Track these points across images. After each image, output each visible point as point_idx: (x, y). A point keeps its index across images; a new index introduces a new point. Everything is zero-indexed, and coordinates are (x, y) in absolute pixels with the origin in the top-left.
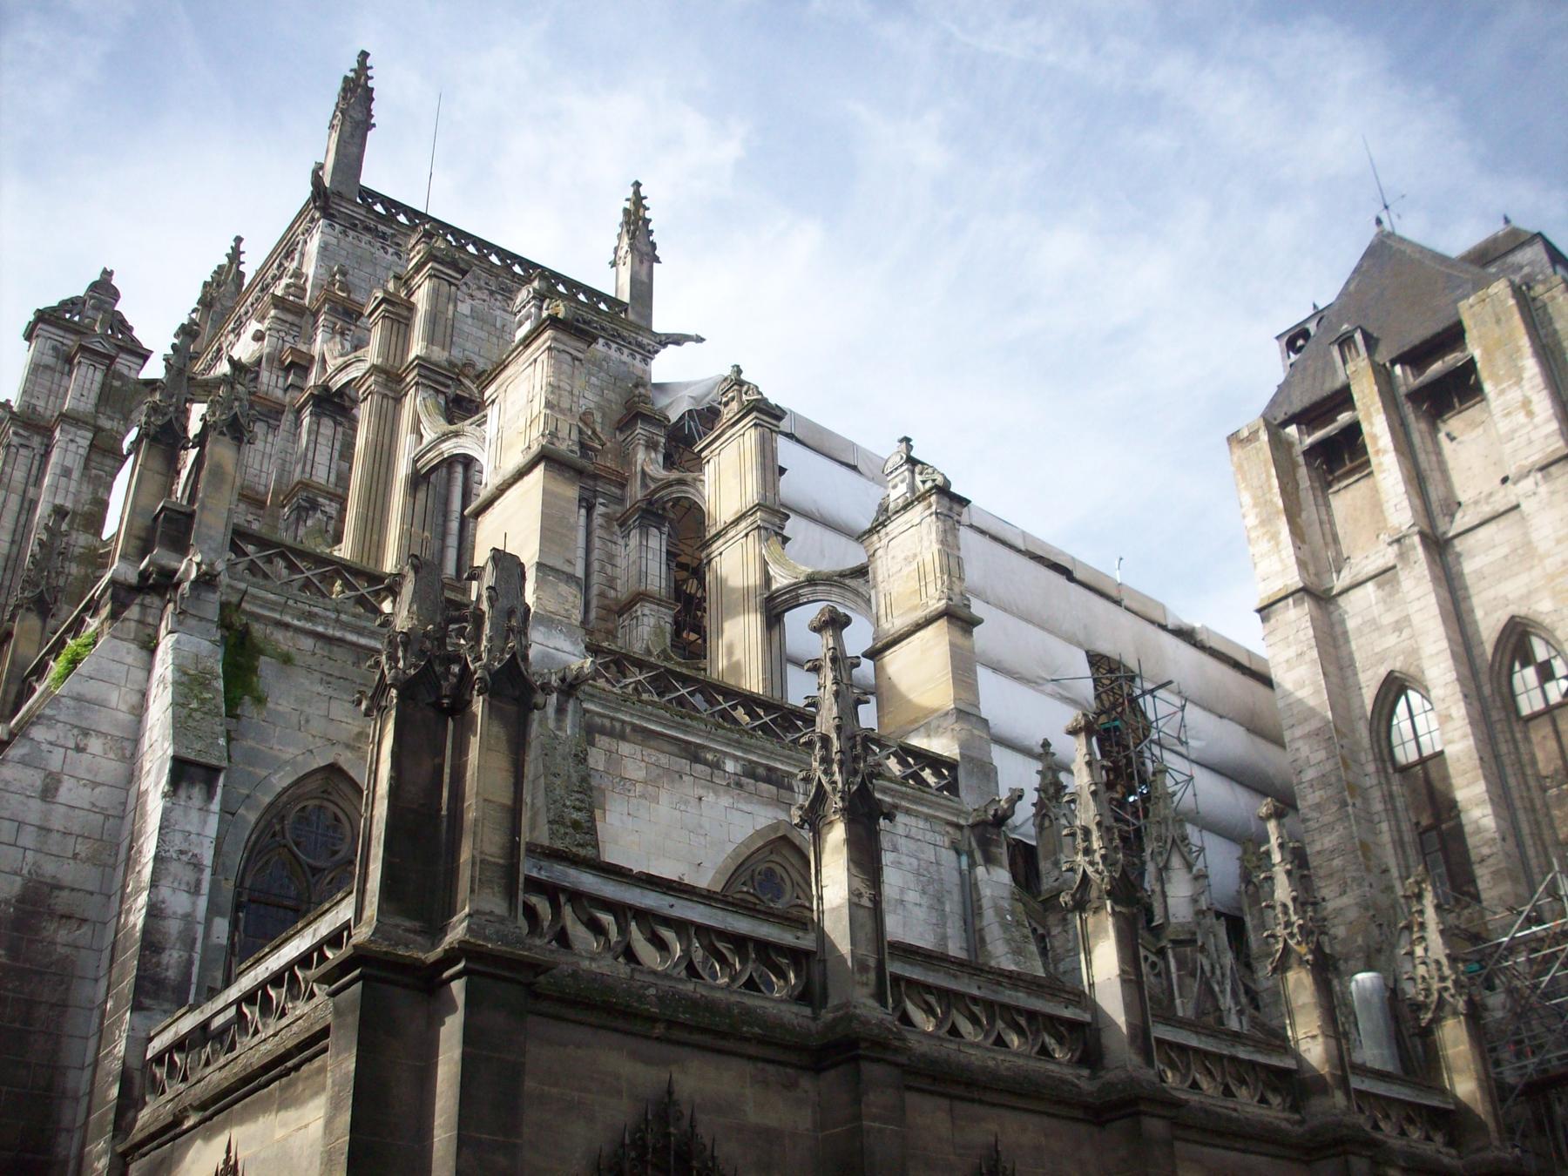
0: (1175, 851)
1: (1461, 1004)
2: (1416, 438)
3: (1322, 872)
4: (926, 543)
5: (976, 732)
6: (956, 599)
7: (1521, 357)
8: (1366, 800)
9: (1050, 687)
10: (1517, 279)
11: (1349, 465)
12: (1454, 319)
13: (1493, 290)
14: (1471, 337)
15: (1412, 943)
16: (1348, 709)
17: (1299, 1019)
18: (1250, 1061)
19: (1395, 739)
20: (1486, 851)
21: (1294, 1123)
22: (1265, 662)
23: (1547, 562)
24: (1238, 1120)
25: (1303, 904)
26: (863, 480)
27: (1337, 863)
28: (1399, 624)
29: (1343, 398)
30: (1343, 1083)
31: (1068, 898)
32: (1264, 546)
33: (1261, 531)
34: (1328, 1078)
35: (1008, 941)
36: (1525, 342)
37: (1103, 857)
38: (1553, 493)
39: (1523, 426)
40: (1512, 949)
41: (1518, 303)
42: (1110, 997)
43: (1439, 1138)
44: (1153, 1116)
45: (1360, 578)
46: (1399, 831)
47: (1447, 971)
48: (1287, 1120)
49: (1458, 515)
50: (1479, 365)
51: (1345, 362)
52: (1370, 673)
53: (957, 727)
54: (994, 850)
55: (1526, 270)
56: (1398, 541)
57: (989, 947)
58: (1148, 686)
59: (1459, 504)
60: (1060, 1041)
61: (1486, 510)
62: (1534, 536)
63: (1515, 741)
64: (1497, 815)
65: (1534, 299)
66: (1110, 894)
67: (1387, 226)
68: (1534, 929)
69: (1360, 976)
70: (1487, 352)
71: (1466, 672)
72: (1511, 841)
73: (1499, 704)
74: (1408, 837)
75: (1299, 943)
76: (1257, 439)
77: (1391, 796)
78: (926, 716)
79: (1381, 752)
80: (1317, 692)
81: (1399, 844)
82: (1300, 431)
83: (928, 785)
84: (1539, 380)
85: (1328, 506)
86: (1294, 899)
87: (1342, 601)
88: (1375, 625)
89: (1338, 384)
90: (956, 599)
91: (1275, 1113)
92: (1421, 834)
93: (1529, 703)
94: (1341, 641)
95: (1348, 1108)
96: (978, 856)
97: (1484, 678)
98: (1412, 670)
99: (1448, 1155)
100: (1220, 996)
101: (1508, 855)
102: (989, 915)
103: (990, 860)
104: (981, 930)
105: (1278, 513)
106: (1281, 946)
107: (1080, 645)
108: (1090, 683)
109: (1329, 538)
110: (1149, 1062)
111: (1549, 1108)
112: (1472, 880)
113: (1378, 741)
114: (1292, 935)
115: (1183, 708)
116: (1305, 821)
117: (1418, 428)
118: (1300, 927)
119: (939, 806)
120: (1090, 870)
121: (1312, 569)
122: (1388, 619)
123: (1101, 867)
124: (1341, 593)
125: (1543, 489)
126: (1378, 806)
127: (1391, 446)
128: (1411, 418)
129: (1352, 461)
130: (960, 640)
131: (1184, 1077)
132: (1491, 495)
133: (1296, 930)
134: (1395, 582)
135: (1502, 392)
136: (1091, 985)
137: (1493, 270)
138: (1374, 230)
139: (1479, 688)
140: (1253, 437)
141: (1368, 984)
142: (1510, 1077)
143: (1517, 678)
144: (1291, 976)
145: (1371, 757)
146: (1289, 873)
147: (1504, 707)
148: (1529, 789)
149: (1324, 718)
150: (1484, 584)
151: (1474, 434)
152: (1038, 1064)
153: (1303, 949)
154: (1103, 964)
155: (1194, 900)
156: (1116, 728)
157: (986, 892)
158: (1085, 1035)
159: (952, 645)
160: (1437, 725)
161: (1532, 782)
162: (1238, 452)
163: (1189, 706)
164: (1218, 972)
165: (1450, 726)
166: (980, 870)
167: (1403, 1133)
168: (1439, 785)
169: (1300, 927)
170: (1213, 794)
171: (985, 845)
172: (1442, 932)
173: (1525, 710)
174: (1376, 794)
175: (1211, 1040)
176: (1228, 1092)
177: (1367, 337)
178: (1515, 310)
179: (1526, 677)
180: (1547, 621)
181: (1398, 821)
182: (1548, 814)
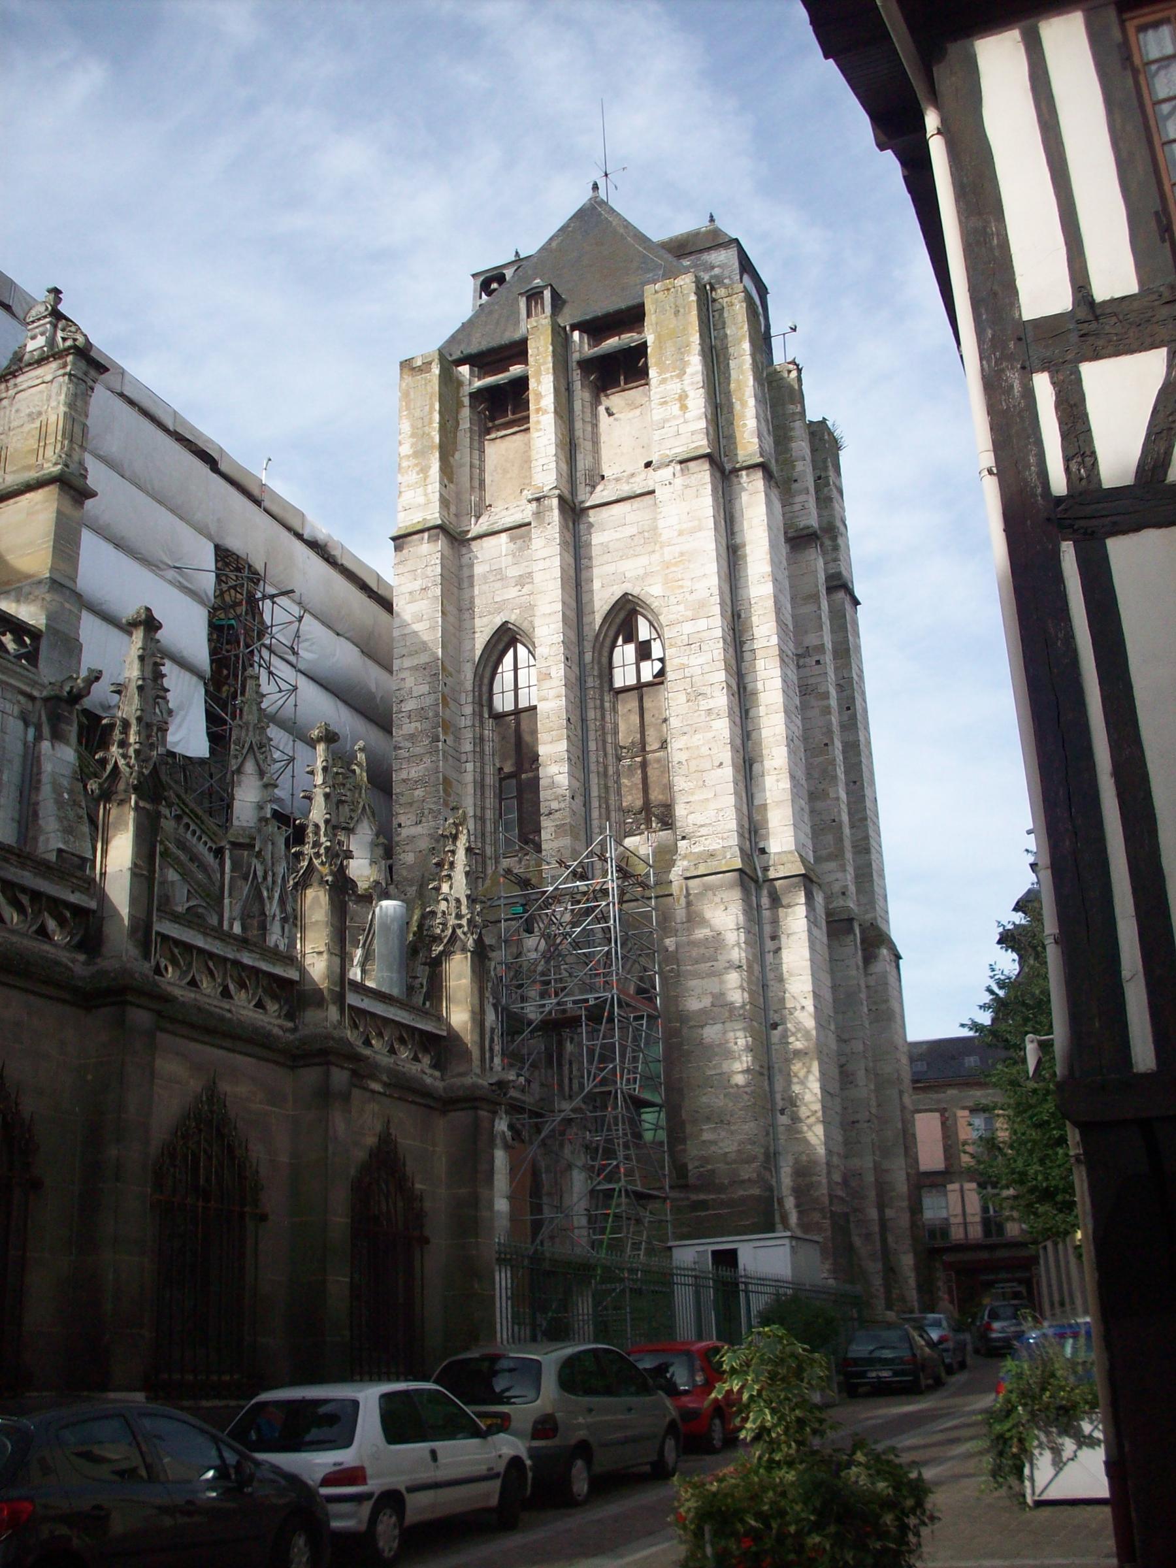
0: (250, 756)
1: (470, 943)
2: (577, 406)
3: (402, 800)
4: (54, 404)
5: (67, 605)
6: (73, 467)
7: (689, 352)
8: (458, 739)
9: (171, 574)
10: (706, 277)
11: (510, 417)
12: (631, 302)
13: (679, 282)
14: (650, 319)
15: (441, 880)
16: (459, 648)
17: (310, 935)
18: (253, 967)
19: (497, 688)
20: (555, 805)
21: (285, 1030)
22: (390, 588)
23: (666, 550)
24: (230, 1020)
25: (335, 828)
26: (15, 322)
27: (419, 793)
28: (521, 580)
29: (518, 351)
30: (340, 999)
31: (95, 786)
32: (413, 477)
33: (413, 461)
34: (326, 993)
35: (60, 819)
36: (695, 338)
37: (137, 752)
38: (687, 486)
39: (675, 417)
40: (556, 897)
41: (699, 301)
42: (119, 891)
43: (426, 1060)
44: (139, 1006)
45: (496, 528)
46: (483, 773)
47: (464, 910)
48: (280, 1027)
49: (599, 488)
50: (649, 350)
51: (529, 315)
52: (485, 620)
53: (48, 597)
54: (63, 726)
55: (717, 271)
56: (538, 500)
57: (40, 822)
58: (271, 590)
59: (603, 477)
60: (62, 922)
61: (625, 489)
62: (661, 524)
63: (602, 707)
64: (571, 774)
65: (714, 300)
66: (136, 789)
67: (602, 194)
68: (578, 883)
69: (385, 903)
70: (659, 338)
71: (573, 636)
72: (579, 800)
73: (596, 673)
74: (489, 780)
75: (322, 864)
76: (429, 371)
77: (482, 739)
78: (19, 581)
79: (480, 696)
80: (433, 628)
81: (480, 785)
82: (471, 372)
83: (7, 651)
84: (699, 378)
85: (482, 451)
86: (327, 822)
87: (475, 545)
88: (499, 575)
89: (517, 336)
90: (73, 467)
91: (271, 1019)
92: (501, 780)
93: (623, 677)
94: (465, 585)
95: (340, 1022)
96: (46, 730)
97: (588, 646)
98: (525, 626)
99: (431, 1076)
100: (267, 901)
101: (574, 813)
102: (46, 791)
103: (57, 736)
104: (37, 803)
105: (433, 447)
106: (306, 863)
107: (209, 537)
108: (212, 577)
109: (476, 484)
110: (146, 956)
111: (560, 1043)
112: (538, 830)
113: (480, 686)
114: (318, 855)
115: (300, 619)
116: (397, 748)
117: (582, 396)
118: (327, 848)
119: (15, 674)
120: (121, 762)
121: (453, 509)
122: (513, 572)
123: (133, 761)
124: (474, 539)
125: (679, 481)
126: (468, 747)
127: (551, 408)
128: (578, 385)
129: (513, 414)
130: (69, 508)
131: (184, 974)
132: (633, 475)
133: (322, 851)
134: (527, 538)
135: (664, 381)
136: (103, 874)
137: (686, 263)
138: (590, 194)
139: (581, 654)
140: (426, 367)
141: (391, 911)
142: (532, 1012)
143: (617, 651)
144: (310, 893)
145: (470, 699)
146: (327, 796)
147: (600, 676)
148: (605, 755)
149: (434, 654)
150: (607, 557)
151: (631, 415)
152: (35, 944)
153: (325, 870)
154: (119, 854)
155: (260, 807)
156: (231, 627)
157: (47, 767)
158: (88, 923)
159: (59, 513)
160: (539, 681)
161: (610, 750)
162: (408, 379)
163: (307, 618)
164: (270, 879)
165: (547, 684)
166: (46, 745)
167: (392, 1051)
168: (527, 738)
169: (327, 848)
170: (317, 707)
171: (56, 721)
172: (467, 874)
173: (618, 683)
174: (468, 735)
175: (218, 943)
176: (226, 994)
177: (555, 296)
178: (695, 305)
179: (625, 653)
180: (655, 604)
181: (483, 765)
182: (617, 782)
